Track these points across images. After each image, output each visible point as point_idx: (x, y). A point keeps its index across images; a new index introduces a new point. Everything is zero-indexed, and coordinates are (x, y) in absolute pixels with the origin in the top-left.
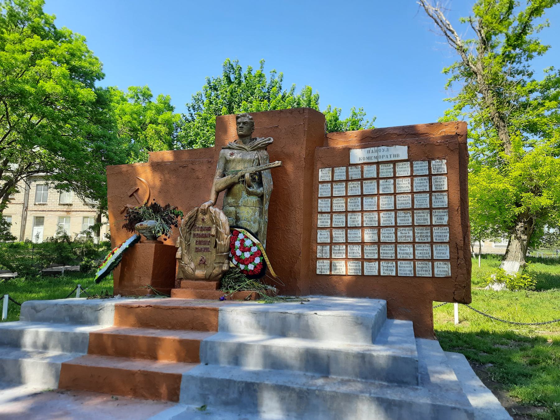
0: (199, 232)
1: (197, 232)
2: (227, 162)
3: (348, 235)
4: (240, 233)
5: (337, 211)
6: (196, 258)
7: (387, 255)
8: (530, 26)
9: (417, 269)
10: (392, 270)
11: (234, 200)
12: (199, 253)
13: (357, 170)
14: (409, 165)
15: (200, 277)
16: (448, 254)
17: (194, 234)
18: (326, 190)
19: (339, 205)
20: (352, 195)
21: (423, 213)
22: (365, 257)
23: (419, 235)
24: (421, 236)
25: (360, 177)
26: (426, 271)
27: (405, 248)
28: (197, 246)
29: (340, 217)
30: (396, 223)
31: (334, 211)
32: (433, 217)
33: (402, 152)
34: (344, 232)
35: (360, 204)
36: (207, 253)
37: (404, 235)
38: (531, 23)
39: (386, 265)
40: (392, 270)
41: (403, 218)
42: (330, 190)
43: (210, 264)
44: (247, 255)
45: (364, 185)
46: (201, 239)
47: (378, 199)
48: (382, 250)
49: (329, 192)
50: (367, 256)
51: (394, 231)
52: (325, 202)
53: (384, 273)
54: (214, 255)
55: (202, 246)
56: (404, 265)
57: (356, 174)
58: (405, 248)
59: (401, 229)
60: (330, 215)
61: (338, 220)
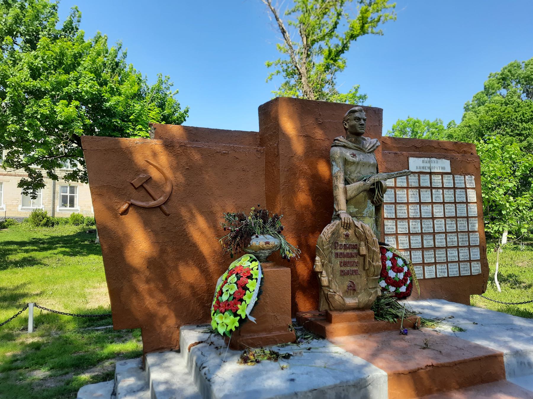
0: (342, 251)
1: (339, 251)
2: (346, 162)
3: (411, 241)
4: (388, 250)
5: (400, 217)
6: (342, 284)
7: (441, 259)
8: (348, 47)
9: (461, 269)
10: (444, 272)
11: (357, 210)
12: (346, 277)
13: (415, 178)
14: (452, 178)
15: (352, 307)
16: (479, 256)
17: (337, 254)
18: (390, 196)
19: (402, 211)
20: (412, 202)
21: (463, 220)
22: (425, 262)
23: (461, 239)
24: (462, 241)
25: (418, 186)
26: (467, 270)
27: (452, 252)
28: (342, 268)
29: (404, 224)
30: (446, 229)
31: (398, 217)
32: (469, 224)
33: (445, 165)
34: (408, 238)
35: (419, 211)
36: (356, 276)
37: (451, 240)
38: (349, 45)
39: (440, 268)
40: (444, 272)
41: (450, 225)
42: (394, 196)
43: (361, 289)
44: (401, 276)
45: (421, 193)
46: (346, 259)
47: (432, 207)
48: (437, 254)
49: (393, 198)
50: (427, 260)
51: (444, 237)
52: (390, 208)
53: (439, 275)
54: (364, 278)
55: (348, 268)
56: (452, 267)
57: (414, 182)
58: (452, 252)
59: (450, 234)
60: (395, 221)
61: (402, 227)
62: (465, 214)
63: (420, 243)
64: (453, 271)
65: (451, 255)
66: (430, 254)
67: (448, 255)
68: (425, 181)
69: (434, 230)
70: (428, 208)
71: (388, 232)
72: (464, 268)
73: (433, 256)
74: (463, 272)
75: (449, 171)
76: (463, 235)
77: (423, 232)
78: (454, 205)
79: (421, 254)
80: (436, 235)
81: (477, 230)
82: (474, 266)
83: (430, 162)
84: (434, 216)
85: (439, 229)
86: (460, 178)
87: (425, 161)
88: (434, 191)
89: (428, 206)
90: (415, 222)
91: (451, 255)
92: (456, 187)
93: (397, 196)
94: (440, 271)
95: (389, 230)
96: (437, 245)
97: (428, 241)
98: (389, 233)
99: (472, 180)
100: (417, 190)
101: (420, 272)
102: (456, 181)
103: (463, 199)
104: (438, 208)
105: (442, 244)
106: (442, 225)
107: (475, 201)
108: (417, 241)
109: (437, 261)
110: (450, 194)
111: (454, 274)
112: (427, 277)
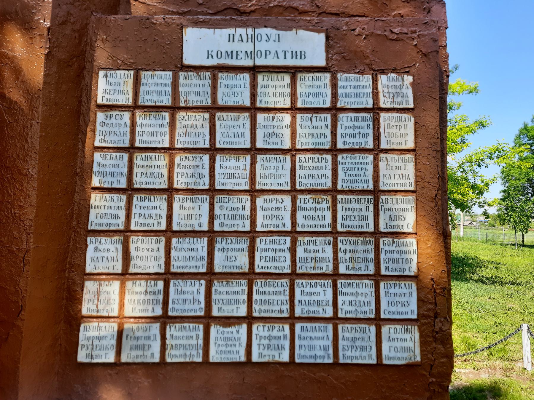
5: (144, 186)
7: (271, 307)
9: (341, 343)
10: (280, 348)
13: (201, 82)
16: (414, 306)
20: (186, 146)
21: (358, 201)
22: (215, 313)
24: (351, 259)
26: (363, 348)
27: (313, 290)
30: (294, 224)
31: (135, 186)
32: (381, 213)
37: (312, 255)
39: (266, 334)
40: (280, 348)
41: (312, 213)
47: (253, 163)
48: (258, 292)
49: (125, 134)
50: (220, 309)
51: (288, 245)
53: (260, 355)
56: (309, 334)
57: (198, 94)
58: (313, 290)
59: (306, 239)
62: (367, 181)
63: (202, 258)
64: (311, 348)
65: (307, 298)
66: (234, 293)
67: (255, 297)
68: (235, 90)
69: (253, 223)
70: (241, 164)
71: (100, 225)
72: (354, 340)
73: (245, 297)
74: (349, 353)
75: (322, 63)
76: (355, 243)
77: (217, 228)
78: (329, 157)
79: (203, 289)
80: (258, 240)
81: (410, 231)
82: (393, 336)
83: (253, 39)
84: (258, 187)
85: (269, 222)
86: (357, 80)
87: (237, 38)
88: (260, 117)
89: (238, 160)
90: (191, 200)
91: (307, 298)
92: (339, 105)
93: (138, 129)
94: (266, 342)
95: (104, 221)
96: (260, 265)
97: (230, 254)
98: (104, 228)
99: (401, 87)
100: (207, 115)
101: (193, 342)
102: (340, 91)
103: (362, 140)
104: (274, 164)
105: (278, 264)
106: (283, 212)
107: (411, 145)
108: (193, 254)
109: (255, 314)
110: (317, 127)
111: (315, 357)
112: (214, 356)
